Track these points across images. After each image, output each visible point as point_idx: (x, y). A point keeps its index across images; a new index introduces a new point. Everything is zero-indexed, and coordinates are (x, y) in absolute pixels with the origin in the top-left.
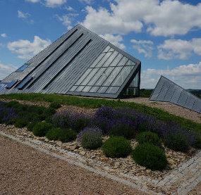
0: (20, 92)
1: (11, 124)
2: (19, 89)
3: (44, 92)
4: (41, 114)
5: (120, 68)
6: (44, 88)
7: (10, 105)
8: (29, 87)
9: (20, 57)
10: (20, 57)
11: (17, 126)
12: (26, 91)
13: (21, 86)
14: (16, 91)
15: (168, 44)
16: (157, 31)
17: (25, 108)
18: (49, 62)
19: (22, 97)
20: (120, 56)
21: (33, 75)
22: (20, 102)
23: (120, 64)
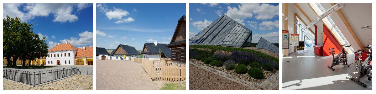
0: (198, 44)
1: (194, 59)
2: (198, 43)
3: (209, 44)
12: (201, 44)
13: (198, 42)
14: (196, 44)
16: (259, 17)
17: (200, 52)
19: (199, 47)
21: (204, 37)
22: (198, 49)
23: (242, 32)
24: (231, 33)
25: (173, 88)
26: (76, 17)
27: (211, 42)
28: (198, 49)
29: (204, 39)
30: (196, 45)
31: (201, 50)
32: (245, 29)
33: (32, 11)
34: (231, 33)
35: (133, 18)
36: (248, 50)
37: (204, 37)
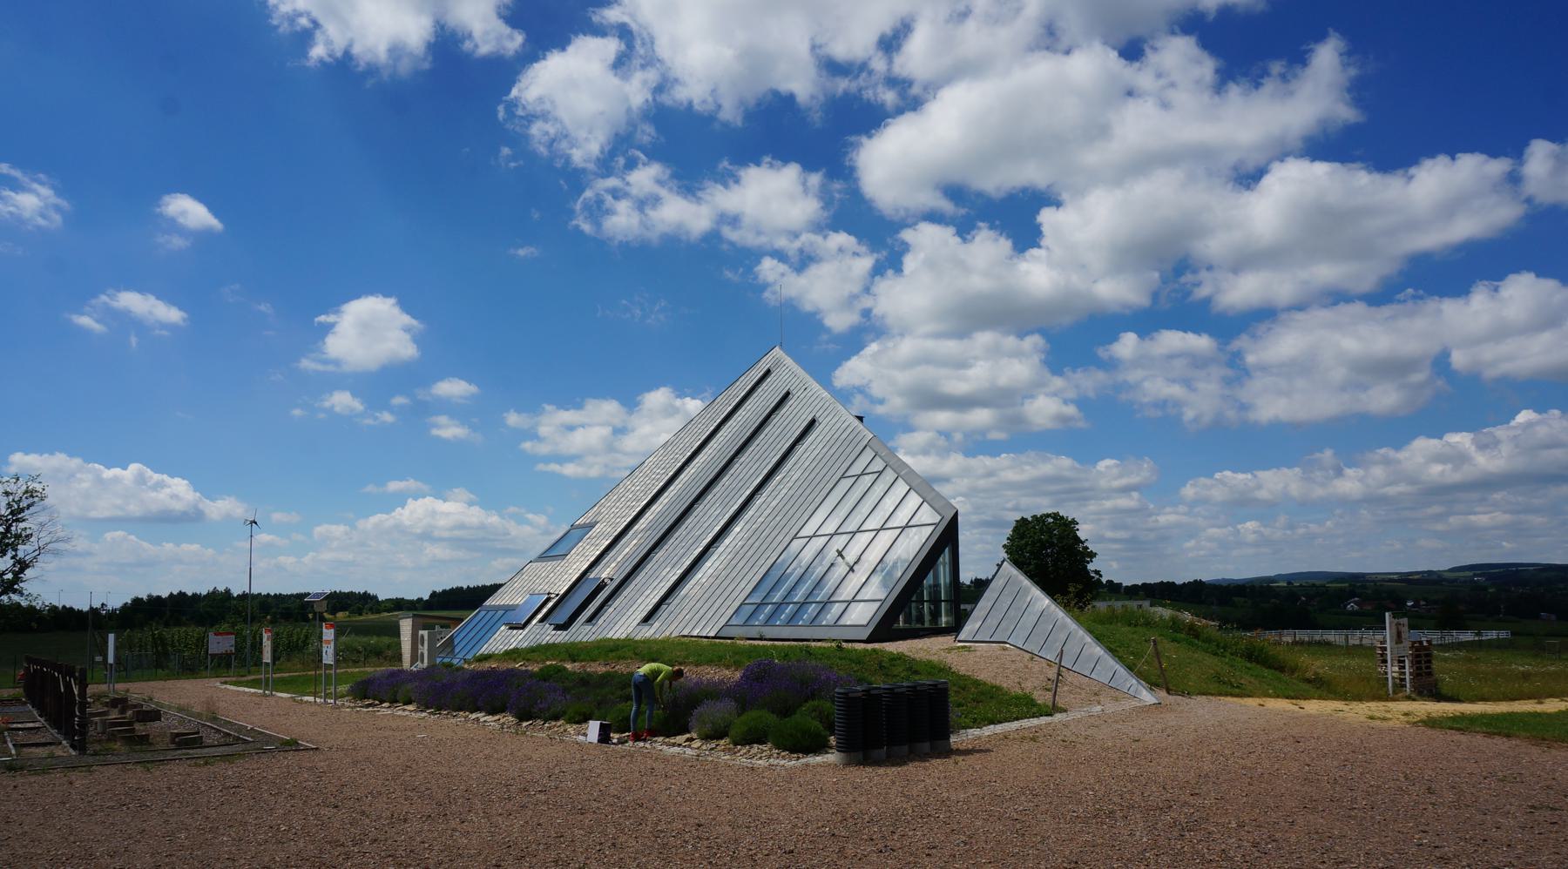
0: (561, 637)
1: (556, 718)
2: (558, 627)
3: (648, 632)
4: (720, 658)
5: (845, 538)
6: (647, 619)
7: (545, 676)
8: (590, 620)
9: (570, 470)
10: (570, 470)
11: (571, 721)
12: (581, 633)
13: (562, 616)
14: (548, 635)
15: (1285, 344)
16: (1243, 291)
17: (585, 681)
18: (684, 504)
19: (573, 652)
20: (902, 487)
21: (605, 572)
22: (569, 666)
23: (823, 540)
24: (808, 530)
25: (1282, 519)
26: (473, 389)
27: (665, 612)
28: (569, 666)
29: (540, 616)
30: (549, 647)
31: (589, 674)
32: (912, 493)
33: (1254, 336)
34: (808, 530)
35: (470, 382)
36: (912, 666)
37: (605, 572)
